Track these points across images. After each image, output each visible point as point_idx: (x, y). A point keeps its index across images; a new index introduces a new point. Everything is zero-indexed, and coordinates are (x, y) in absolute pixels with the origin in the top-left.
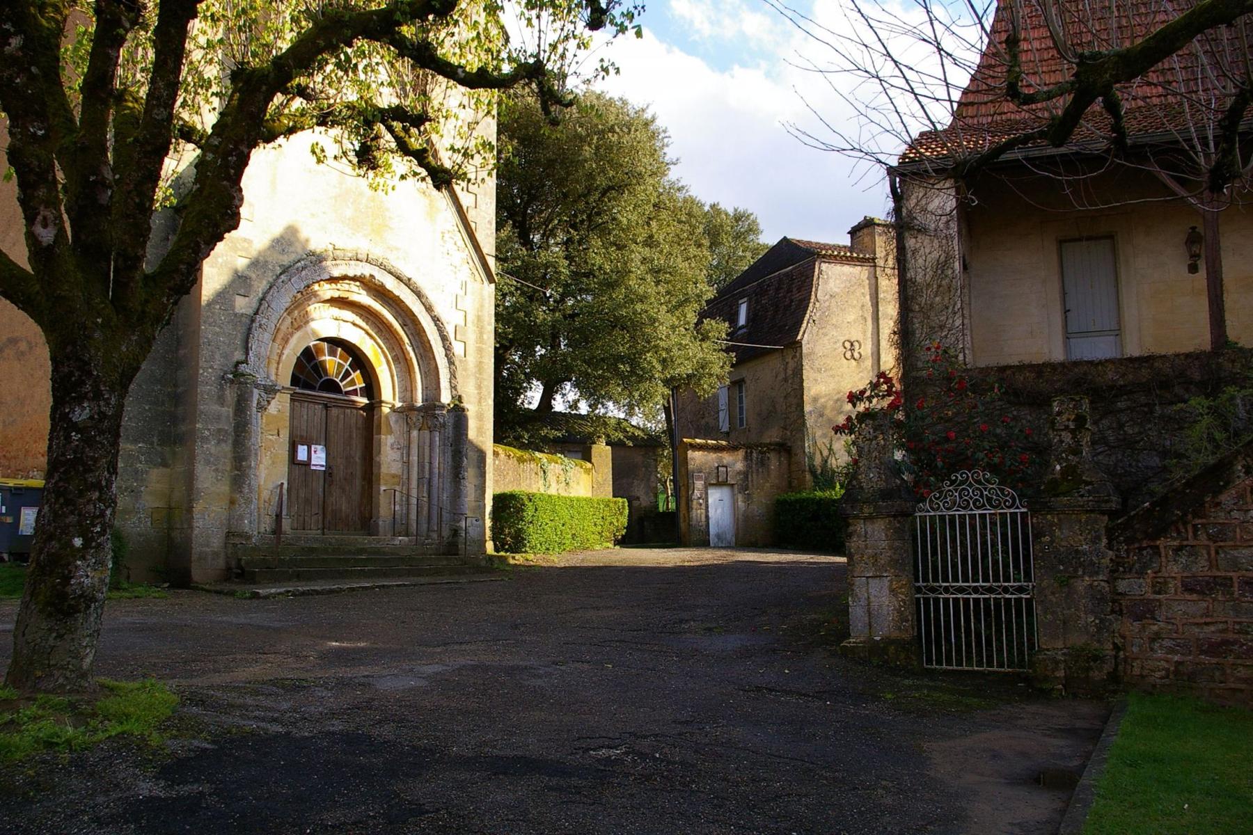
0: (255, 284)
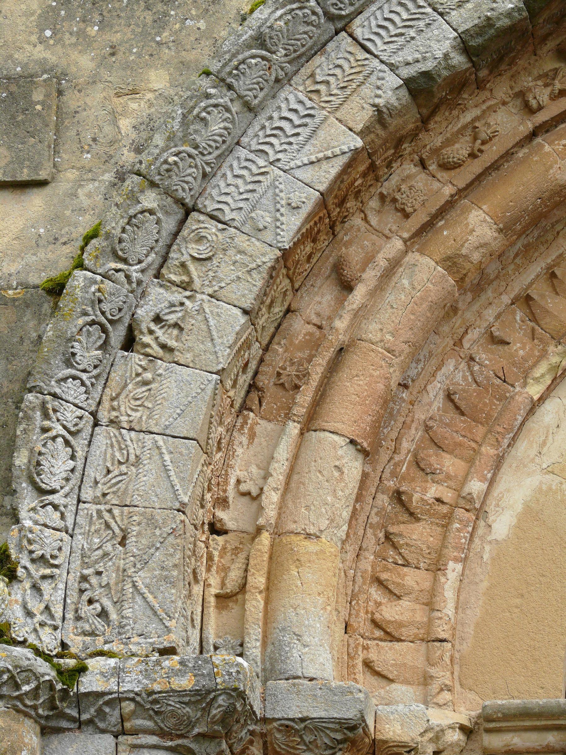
0: (91, 105)
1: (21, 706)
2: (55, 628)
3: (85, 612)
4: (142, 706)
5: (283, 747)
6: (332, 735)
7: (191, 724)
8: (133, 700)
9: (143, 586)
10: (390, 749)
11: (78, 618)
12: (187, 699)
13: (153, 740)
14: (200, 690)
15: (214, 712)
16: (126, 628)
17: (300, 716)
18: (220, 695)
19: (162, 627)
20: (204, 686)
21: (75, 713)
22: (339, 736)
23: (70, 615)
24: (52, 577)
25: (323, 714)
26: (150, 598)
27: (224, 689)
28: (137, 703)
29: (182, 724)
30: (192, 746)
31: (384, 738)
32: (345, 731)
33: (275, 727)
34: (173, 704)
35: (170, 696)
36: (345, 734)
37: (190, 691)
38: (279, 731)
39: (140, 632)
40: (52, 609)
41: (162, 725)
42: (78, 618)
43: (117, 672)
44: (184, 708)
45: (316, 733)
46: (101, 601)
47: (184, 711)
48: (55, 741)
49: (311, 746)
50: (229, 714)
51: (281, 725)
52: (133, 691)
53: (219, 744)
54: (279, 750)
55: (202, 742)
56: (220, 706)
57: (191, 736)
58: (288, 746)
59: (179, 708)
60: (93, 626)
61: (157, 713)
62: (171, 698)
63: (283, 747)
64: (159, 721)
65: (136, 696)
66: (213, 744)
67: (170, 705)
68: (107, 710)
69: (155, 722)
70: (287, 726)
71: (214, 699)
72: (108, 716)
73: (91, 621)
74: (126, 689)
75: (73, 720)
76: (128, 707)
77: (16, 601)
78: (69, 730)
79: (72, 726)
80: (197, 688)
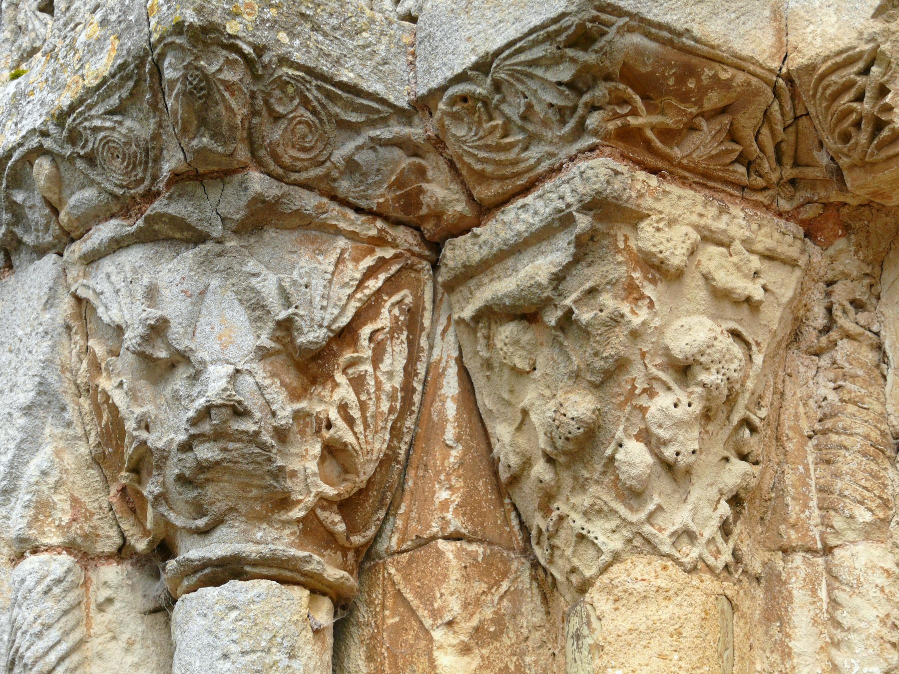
5: (482, 154)
6: (552, 76)
7: (151, 154)
8: (40, 151)
10: (825, 82)
17: (474, 58)
18: (162, 56)
22: (565, 73)
25: (512, 32)
31: (804, 61)
32: (570, 52)
33: (444, 113)
35: (90, 107)
36: (573, 60)
37: (113, 76)
38: (457, 118)
45: (520, 87)
49: (530, 127)
50: (202, 92)
51: (453, 101)
54: (478, 167)
55: (200, 192)
58: (488, 148)
59: (113, 129)
61: (90, 159)
62: (93, 112)
63: (482, 154)
66: (229, 190)
70: (464, 99)
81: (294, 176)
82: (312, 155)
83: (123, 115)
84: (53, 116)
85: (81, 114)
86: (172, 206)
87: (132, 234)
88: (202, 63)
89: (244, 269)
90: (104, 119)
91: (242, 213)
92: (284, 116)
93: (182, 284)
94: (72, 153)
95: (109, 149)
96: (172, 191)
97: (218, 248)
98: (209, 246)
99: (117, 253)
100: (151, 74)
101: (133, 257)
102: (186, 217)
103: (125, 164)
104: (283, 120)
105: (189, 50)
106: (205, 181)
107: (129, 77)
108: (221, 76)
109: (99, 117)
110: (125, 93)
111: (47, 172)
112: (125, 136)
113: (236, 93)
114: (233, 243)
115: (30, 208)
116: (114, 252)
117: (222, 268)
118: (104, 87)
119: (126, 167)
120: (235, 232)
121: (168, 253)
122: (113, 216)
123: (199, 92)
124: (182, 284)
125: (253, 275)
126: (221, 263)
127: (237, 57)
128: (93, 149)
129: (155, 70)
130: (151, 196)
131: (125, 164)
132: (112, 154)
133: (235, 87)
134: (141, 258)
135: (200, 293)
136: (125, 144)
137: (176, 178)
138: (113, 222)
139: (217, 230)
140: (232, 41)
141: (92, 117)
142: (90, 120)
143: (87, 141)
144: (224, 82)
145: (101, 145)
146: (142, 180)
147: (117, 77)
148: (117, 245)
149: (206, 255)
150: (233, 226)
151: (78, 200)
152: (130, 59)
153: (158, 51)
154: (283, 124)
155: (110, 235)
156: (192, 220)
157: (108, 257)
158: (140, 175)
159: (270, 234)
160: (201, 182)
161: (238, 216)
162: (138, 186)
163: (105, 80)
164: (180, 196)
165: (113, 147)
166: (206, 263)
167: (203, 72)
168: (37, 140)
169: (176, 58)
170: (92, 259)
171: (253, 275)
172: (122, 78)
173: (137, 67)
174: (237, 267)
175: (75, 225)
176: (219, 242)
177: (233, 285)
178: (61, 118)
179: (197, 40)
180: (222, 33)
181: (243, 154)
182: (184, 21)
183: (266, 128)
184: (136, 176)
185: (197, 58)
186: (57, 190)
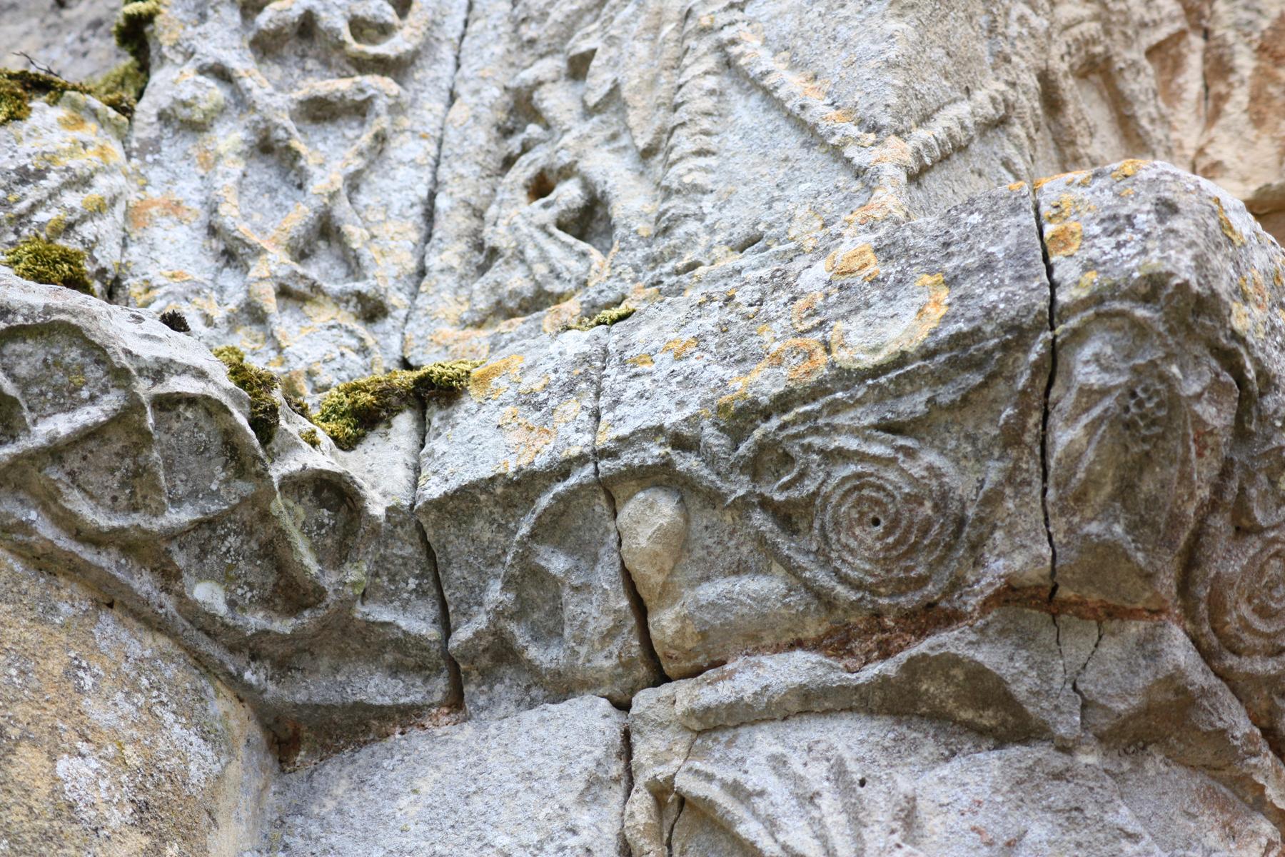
1: (46, 530)
2: (372, 310)
3: (513, 228)
4: (713, 498)
7: (964, 533)
8: (660, 477)
9: (765, 54)
11: (486, 256)
12: (914, 404)
13: (792, 669)
14: (976, 334)
15: (1065, 436)
16: (680, 232)
18: (1078, 336)
19: (842, 179)
20: (988, 313)
21: (417, 623)
23: (448, 254)
24: (360, 109)
26: (791, 85)
27: (1097, 299)
28: (681, 486)
29: (914, 548)
30: (988, 656)
34: (852, 444)
35: (835, 408)
37: (928, 354)
39: (741, 231)
40: (347, 228)
41: (823, 579)
42: (486, 256)
43: (587, 375)
44: (910, 453)
46: (583, 165)
47: (917, 471)
48: (338, 784)
52: (659, 430)
53: (1149, 648)
55: (1047, 635)
56: (1091, 395)
57: (973, 602)
60: (541, 270)
61: (786, 517)
62: (841, 419)
64: (801, 559)
65: (675, 456)
66: (1110, 649)
67: (843, 455)
68: (557, 563)
69: (793, 571)
71: (1052, 367)
72: (566, 594)
73: (531, 253)
74: (624, 431)
75: (405, 656)
76: (649, 518)
77: (174, 207)
78: (408, 716)
79: (416, 697)
80: (963, 326)
81: (1231, 661)
82: (1272, 629)
83: (920, 439)
84: (723, 409)
85: (807, 416)
86: (985, 648)
87: (857, 688)
88: (1175, 369)
89: (1109, 817)
90: (867, 439)
91: (1134, 702)
92: (1260, 531)
93: (975, 813)
94: (749, 493)
95: (860, 501)
96: (990, 617)
97: (1059, 762)
98: (1039, 752)
99: (794, 723)
100: (1037, 368)
101: (847, 737)
102: (1009, 679)
103: (890, 540)
104: (1254, 538)
105: (1159, 335)
106: (1064, 617)
107: (974, 364)
108: (1198, 408)
109: (855, 432)
110: (947, 395)
111: (664, 521)
112: (914, 481)
113: (1207, 453)
114: (1092, 760)
115: (576, 589)
116: (785, 719)
117: (1061, 805)
118: (897, 371)
119: (888, 548)
120: (1101, 738)
121: (930, 748)
122: (798, 644)
123: (1148, 427)
124: (975, 813)
125: (1129, 836)
126: (1061, 794)
127: (1231, 379)
128: (815, 494)
129: (1048, 365)
130: (931, 617)
131: (890, 540)
132: (862, 514)
133: (1210, 440)
134: (862, 742)
135: (1009, 844)
136: (908, 498)
137: (1011, 594)
138: (799, 657)
139: (1068, 724)
140: (1234, 345)
141: (835, 429)
142: (827, 434)
143: (802, 475)
144: (1198, 420)
145: (840, 492)
146: (922, 581)
147: (941, 358)
148: (809, 703)
149: (1030, 769)
150: (1104, 723)
151: (727, 595)
152: (988, 329)
153: (1073, 322)
154: (1253, 546)
155: (797, 680)
156: (1020, 690)
157: (765, 727)
158: (921, 570)
159: (1154, 764)
160: (1054, 616)
161: (1122, 707)
162: (902, 593)
163: (902, 359)
164: (1003, 632)
165: (870, 499)
166: (1028, 785)
167: (1171, 387)
168: (657, 451)
169: (1114, 348)
170: (711, 725)
171: (1129, 836)
172: (952, 362)
173: (1005, 346)
174: (1091, 811)
175: (689, 645)
176: (1065, 748)
177: (1079, 845)
178: (739, 419)
179: (1183, 322)
180: (1224, 326)
181: (1167, 582)
182: (1170, 275)
183: (1222, 543)
184: (908, 569)
185: (1169, 357)
186: (668, 565)
